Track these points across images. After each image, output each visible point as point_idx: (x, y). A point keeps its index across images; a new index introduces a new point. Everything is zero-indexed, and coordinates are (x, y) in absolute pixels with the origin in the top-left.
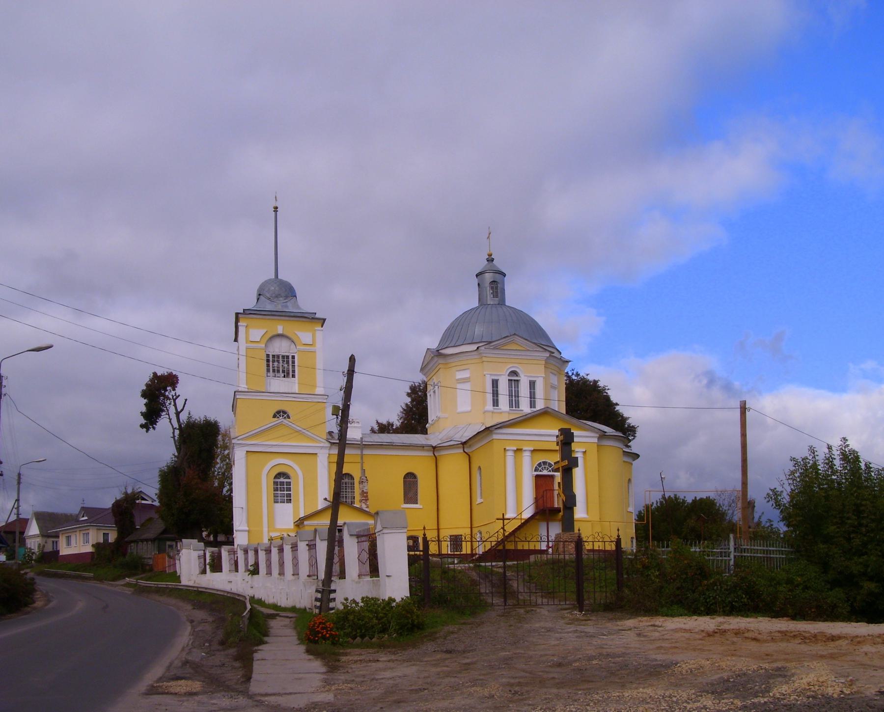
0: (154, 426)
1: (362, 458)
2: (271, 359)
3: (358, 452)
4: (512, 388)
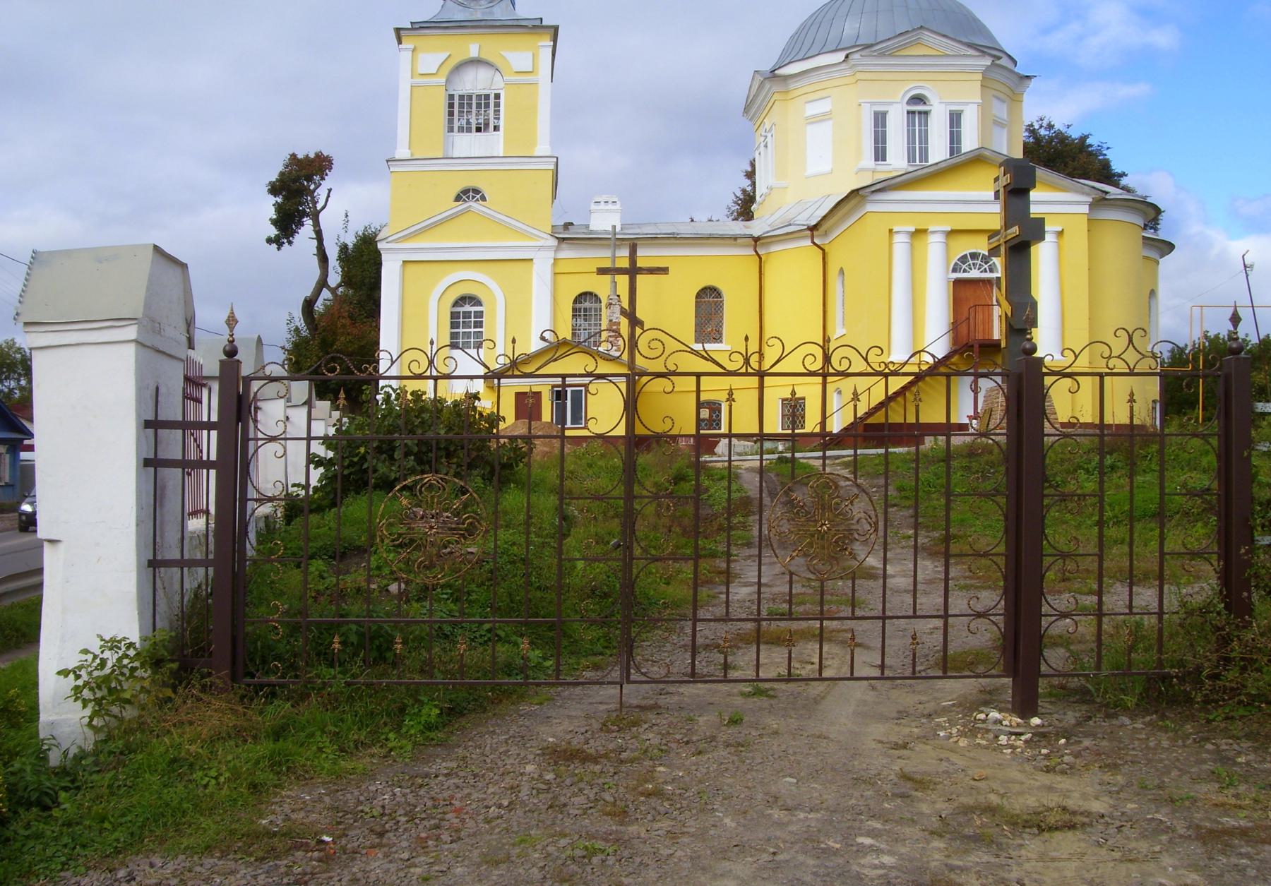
4: (920, 149)
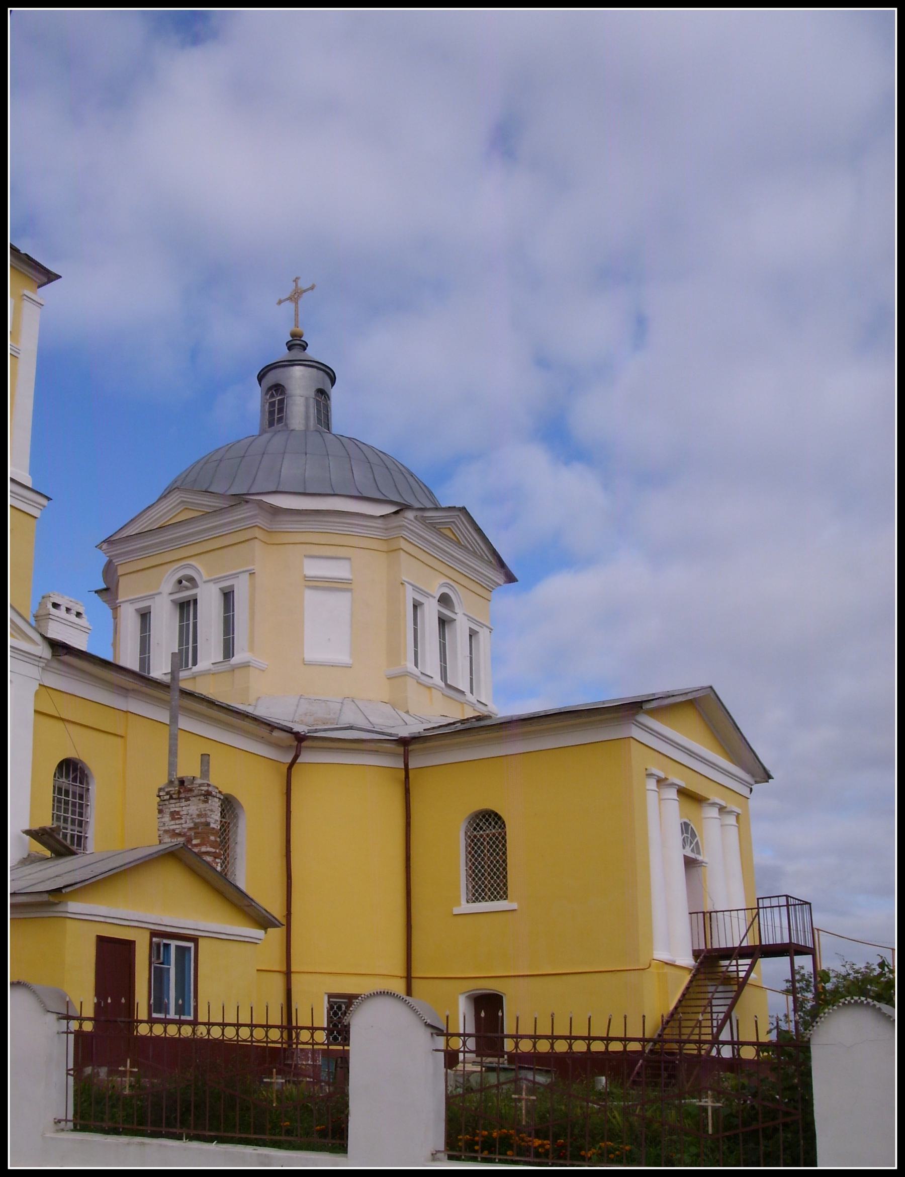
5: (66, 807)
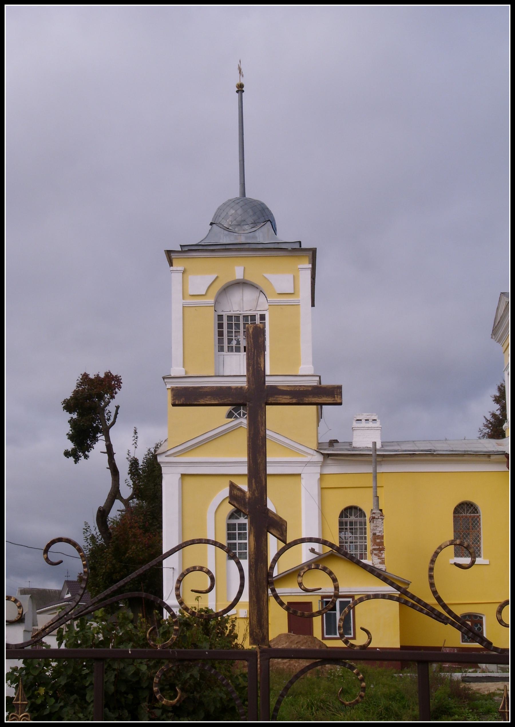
0: (87, 453)
1: (375, 478)
2: (225, 322)
3: (369, 469)
5: (355, 531)
